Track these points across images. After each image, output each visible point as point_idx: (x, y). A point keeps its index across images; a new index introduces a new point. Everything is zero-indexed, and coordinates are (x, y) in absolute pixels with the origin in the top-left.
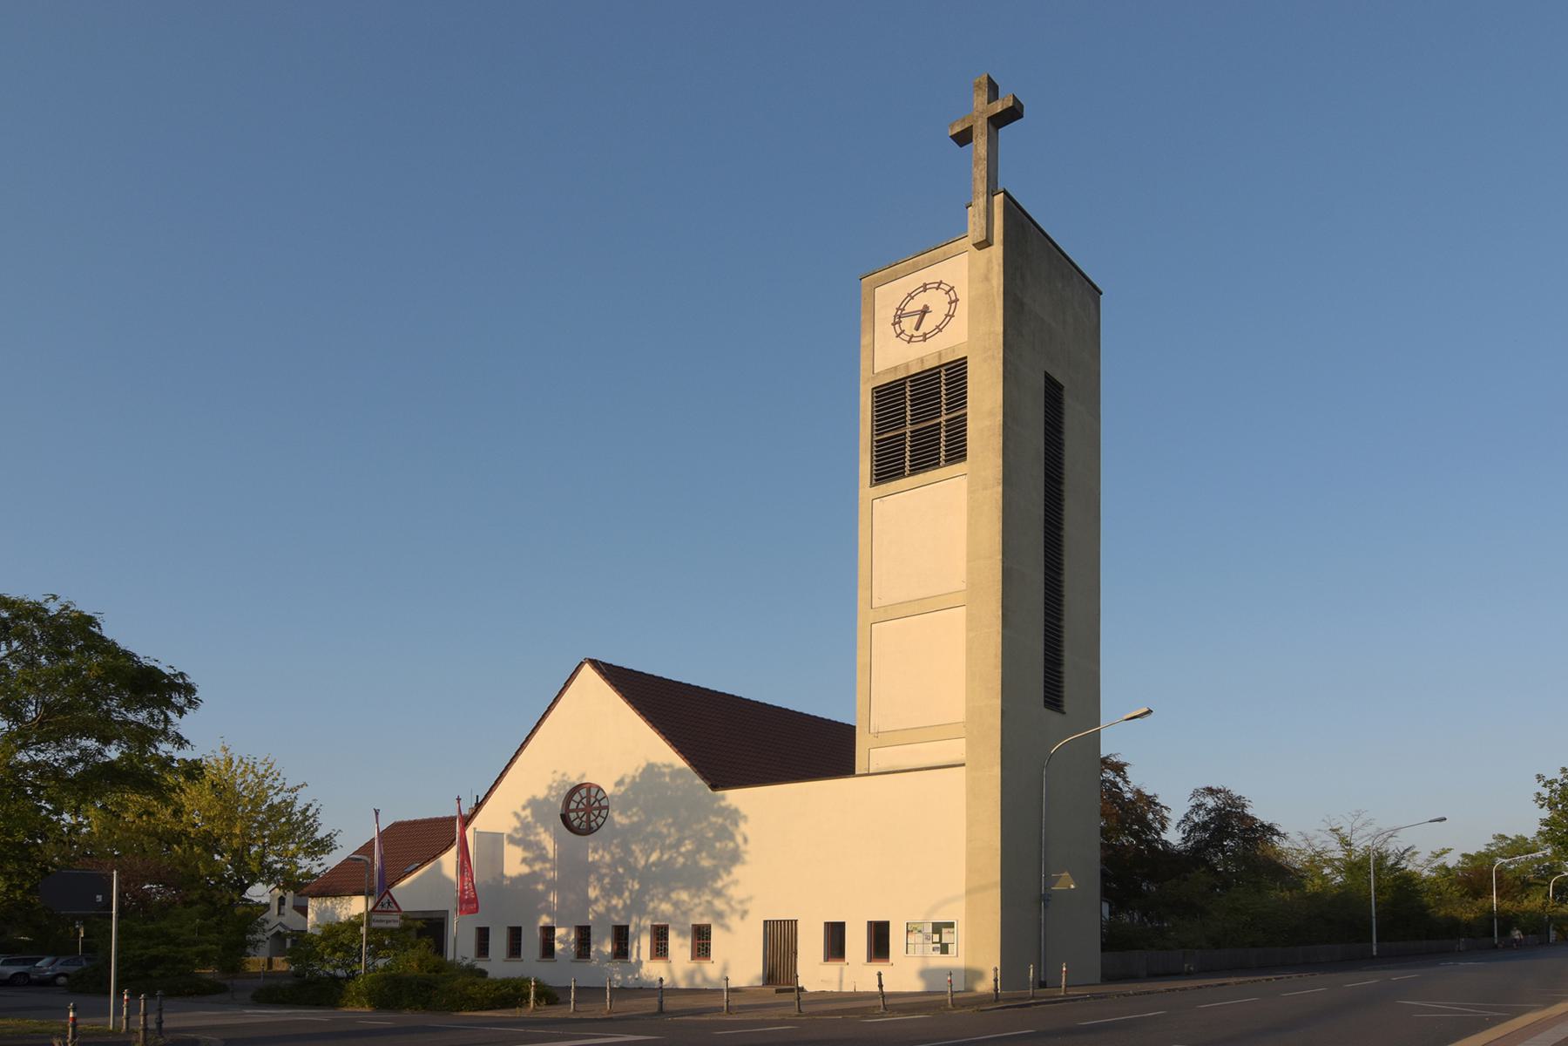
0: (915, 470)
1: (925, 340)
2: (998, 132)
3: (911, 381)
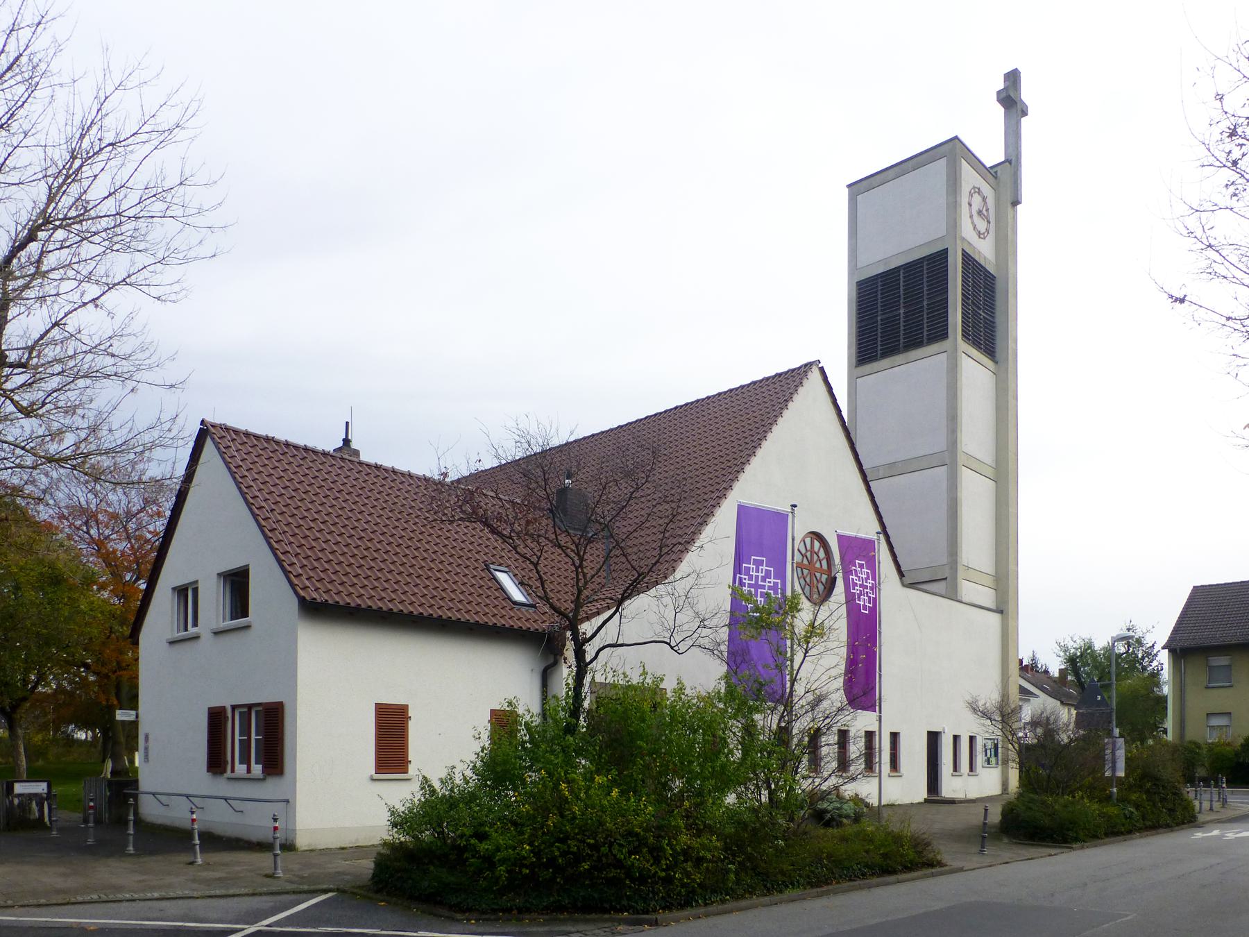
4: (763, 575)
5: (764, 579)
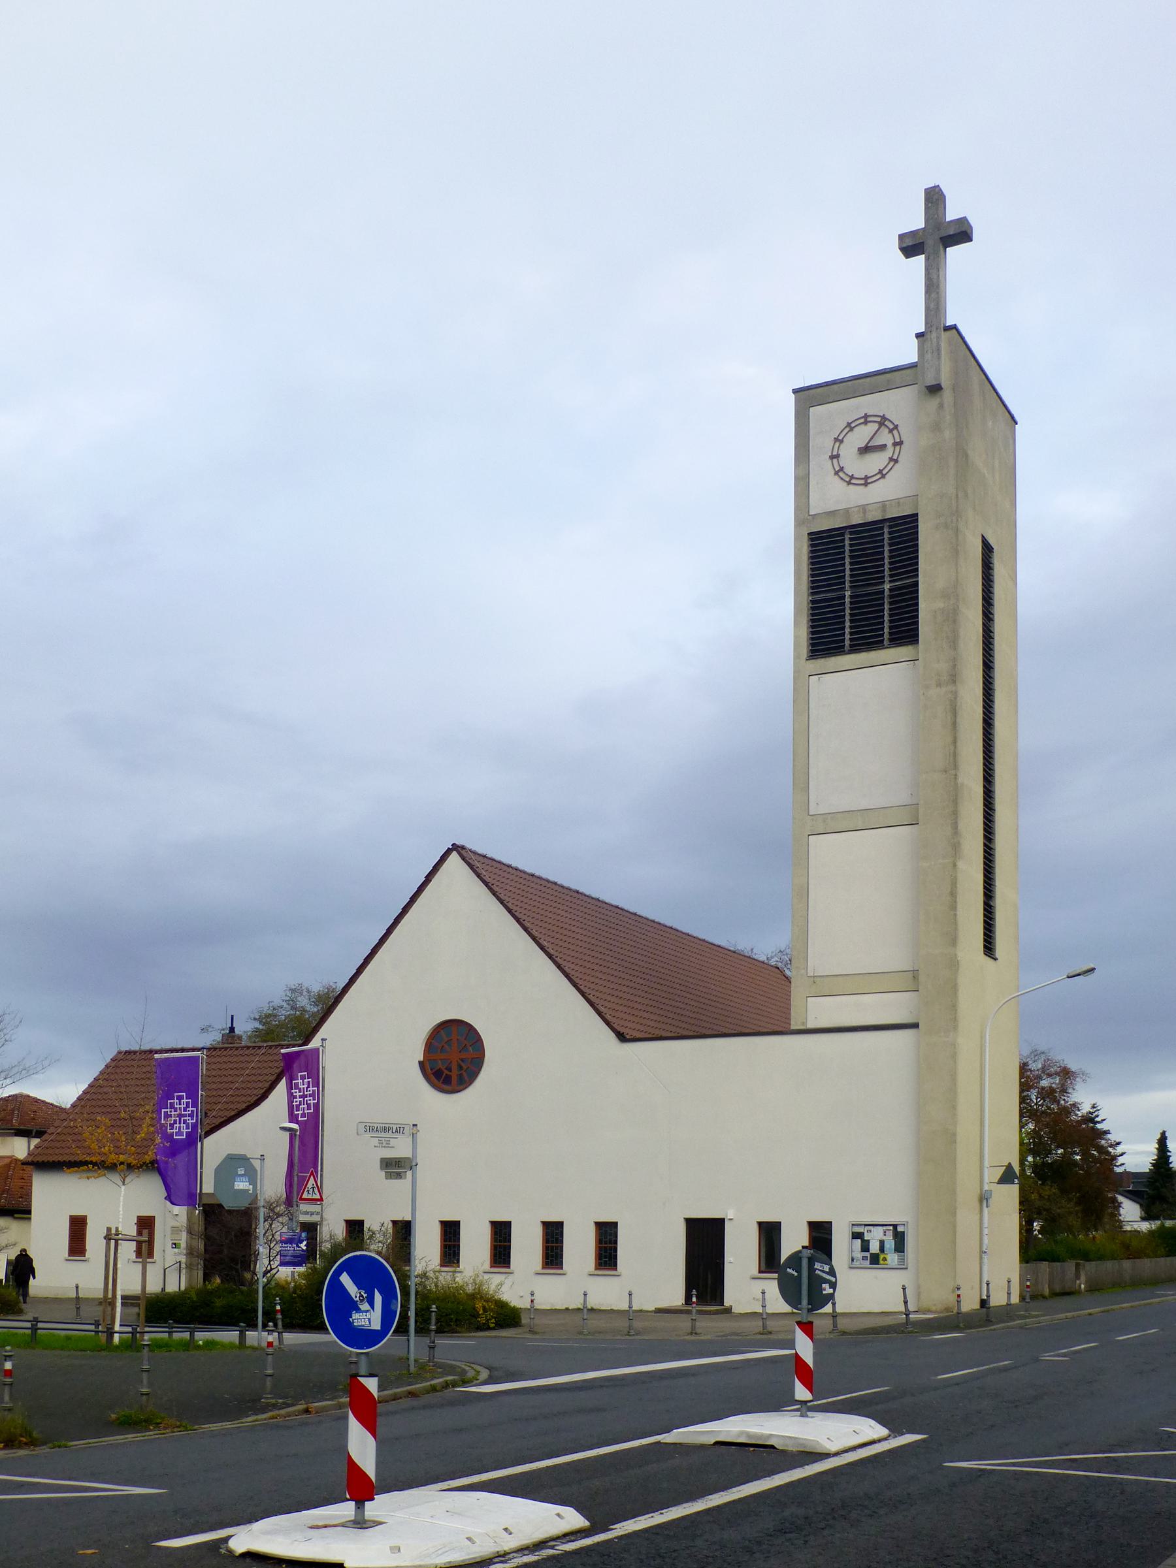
0: (856, 648)
1: (866, 484)
2: (945, 251)
3: (851, 533)
4: (175, 1125)
5: (175, 1122)
